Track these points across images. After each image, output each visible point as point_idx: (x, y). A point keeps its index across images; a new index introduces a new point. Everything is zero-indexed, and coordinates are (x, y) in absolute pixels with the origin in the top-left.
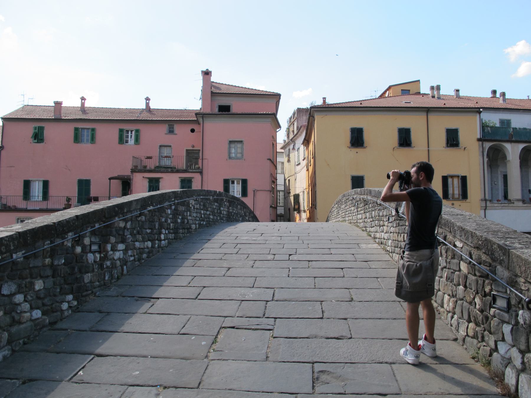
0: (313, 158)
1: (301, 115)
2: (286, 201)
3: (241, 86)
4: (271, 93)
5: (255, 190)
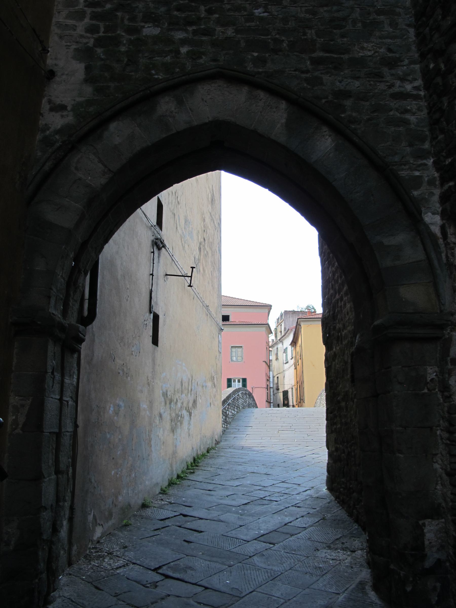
0: (300, 359)
1: (288, 316)
2: (275, 398)
3: (237, 298)
4: (264, 304)
5: (254, 387)
